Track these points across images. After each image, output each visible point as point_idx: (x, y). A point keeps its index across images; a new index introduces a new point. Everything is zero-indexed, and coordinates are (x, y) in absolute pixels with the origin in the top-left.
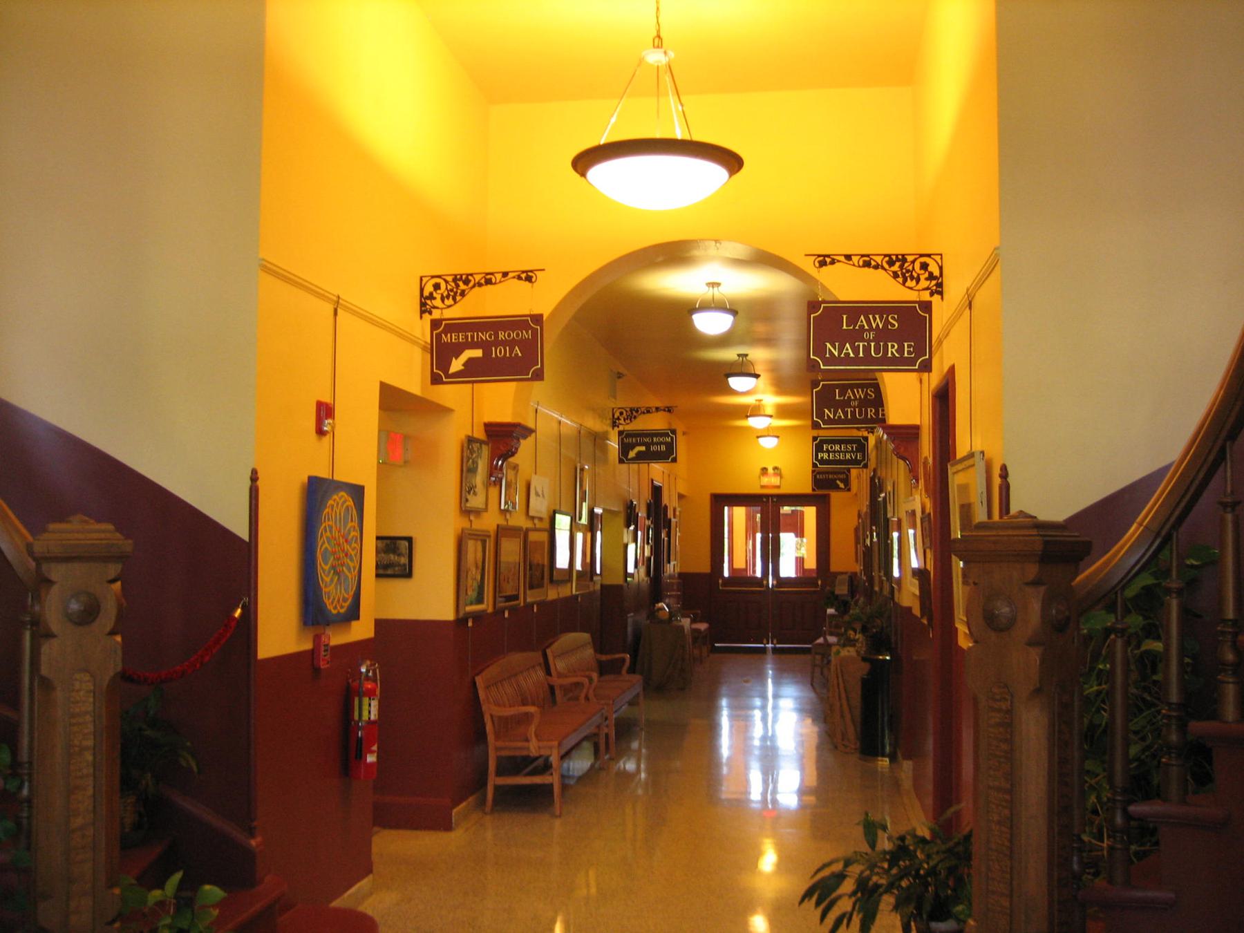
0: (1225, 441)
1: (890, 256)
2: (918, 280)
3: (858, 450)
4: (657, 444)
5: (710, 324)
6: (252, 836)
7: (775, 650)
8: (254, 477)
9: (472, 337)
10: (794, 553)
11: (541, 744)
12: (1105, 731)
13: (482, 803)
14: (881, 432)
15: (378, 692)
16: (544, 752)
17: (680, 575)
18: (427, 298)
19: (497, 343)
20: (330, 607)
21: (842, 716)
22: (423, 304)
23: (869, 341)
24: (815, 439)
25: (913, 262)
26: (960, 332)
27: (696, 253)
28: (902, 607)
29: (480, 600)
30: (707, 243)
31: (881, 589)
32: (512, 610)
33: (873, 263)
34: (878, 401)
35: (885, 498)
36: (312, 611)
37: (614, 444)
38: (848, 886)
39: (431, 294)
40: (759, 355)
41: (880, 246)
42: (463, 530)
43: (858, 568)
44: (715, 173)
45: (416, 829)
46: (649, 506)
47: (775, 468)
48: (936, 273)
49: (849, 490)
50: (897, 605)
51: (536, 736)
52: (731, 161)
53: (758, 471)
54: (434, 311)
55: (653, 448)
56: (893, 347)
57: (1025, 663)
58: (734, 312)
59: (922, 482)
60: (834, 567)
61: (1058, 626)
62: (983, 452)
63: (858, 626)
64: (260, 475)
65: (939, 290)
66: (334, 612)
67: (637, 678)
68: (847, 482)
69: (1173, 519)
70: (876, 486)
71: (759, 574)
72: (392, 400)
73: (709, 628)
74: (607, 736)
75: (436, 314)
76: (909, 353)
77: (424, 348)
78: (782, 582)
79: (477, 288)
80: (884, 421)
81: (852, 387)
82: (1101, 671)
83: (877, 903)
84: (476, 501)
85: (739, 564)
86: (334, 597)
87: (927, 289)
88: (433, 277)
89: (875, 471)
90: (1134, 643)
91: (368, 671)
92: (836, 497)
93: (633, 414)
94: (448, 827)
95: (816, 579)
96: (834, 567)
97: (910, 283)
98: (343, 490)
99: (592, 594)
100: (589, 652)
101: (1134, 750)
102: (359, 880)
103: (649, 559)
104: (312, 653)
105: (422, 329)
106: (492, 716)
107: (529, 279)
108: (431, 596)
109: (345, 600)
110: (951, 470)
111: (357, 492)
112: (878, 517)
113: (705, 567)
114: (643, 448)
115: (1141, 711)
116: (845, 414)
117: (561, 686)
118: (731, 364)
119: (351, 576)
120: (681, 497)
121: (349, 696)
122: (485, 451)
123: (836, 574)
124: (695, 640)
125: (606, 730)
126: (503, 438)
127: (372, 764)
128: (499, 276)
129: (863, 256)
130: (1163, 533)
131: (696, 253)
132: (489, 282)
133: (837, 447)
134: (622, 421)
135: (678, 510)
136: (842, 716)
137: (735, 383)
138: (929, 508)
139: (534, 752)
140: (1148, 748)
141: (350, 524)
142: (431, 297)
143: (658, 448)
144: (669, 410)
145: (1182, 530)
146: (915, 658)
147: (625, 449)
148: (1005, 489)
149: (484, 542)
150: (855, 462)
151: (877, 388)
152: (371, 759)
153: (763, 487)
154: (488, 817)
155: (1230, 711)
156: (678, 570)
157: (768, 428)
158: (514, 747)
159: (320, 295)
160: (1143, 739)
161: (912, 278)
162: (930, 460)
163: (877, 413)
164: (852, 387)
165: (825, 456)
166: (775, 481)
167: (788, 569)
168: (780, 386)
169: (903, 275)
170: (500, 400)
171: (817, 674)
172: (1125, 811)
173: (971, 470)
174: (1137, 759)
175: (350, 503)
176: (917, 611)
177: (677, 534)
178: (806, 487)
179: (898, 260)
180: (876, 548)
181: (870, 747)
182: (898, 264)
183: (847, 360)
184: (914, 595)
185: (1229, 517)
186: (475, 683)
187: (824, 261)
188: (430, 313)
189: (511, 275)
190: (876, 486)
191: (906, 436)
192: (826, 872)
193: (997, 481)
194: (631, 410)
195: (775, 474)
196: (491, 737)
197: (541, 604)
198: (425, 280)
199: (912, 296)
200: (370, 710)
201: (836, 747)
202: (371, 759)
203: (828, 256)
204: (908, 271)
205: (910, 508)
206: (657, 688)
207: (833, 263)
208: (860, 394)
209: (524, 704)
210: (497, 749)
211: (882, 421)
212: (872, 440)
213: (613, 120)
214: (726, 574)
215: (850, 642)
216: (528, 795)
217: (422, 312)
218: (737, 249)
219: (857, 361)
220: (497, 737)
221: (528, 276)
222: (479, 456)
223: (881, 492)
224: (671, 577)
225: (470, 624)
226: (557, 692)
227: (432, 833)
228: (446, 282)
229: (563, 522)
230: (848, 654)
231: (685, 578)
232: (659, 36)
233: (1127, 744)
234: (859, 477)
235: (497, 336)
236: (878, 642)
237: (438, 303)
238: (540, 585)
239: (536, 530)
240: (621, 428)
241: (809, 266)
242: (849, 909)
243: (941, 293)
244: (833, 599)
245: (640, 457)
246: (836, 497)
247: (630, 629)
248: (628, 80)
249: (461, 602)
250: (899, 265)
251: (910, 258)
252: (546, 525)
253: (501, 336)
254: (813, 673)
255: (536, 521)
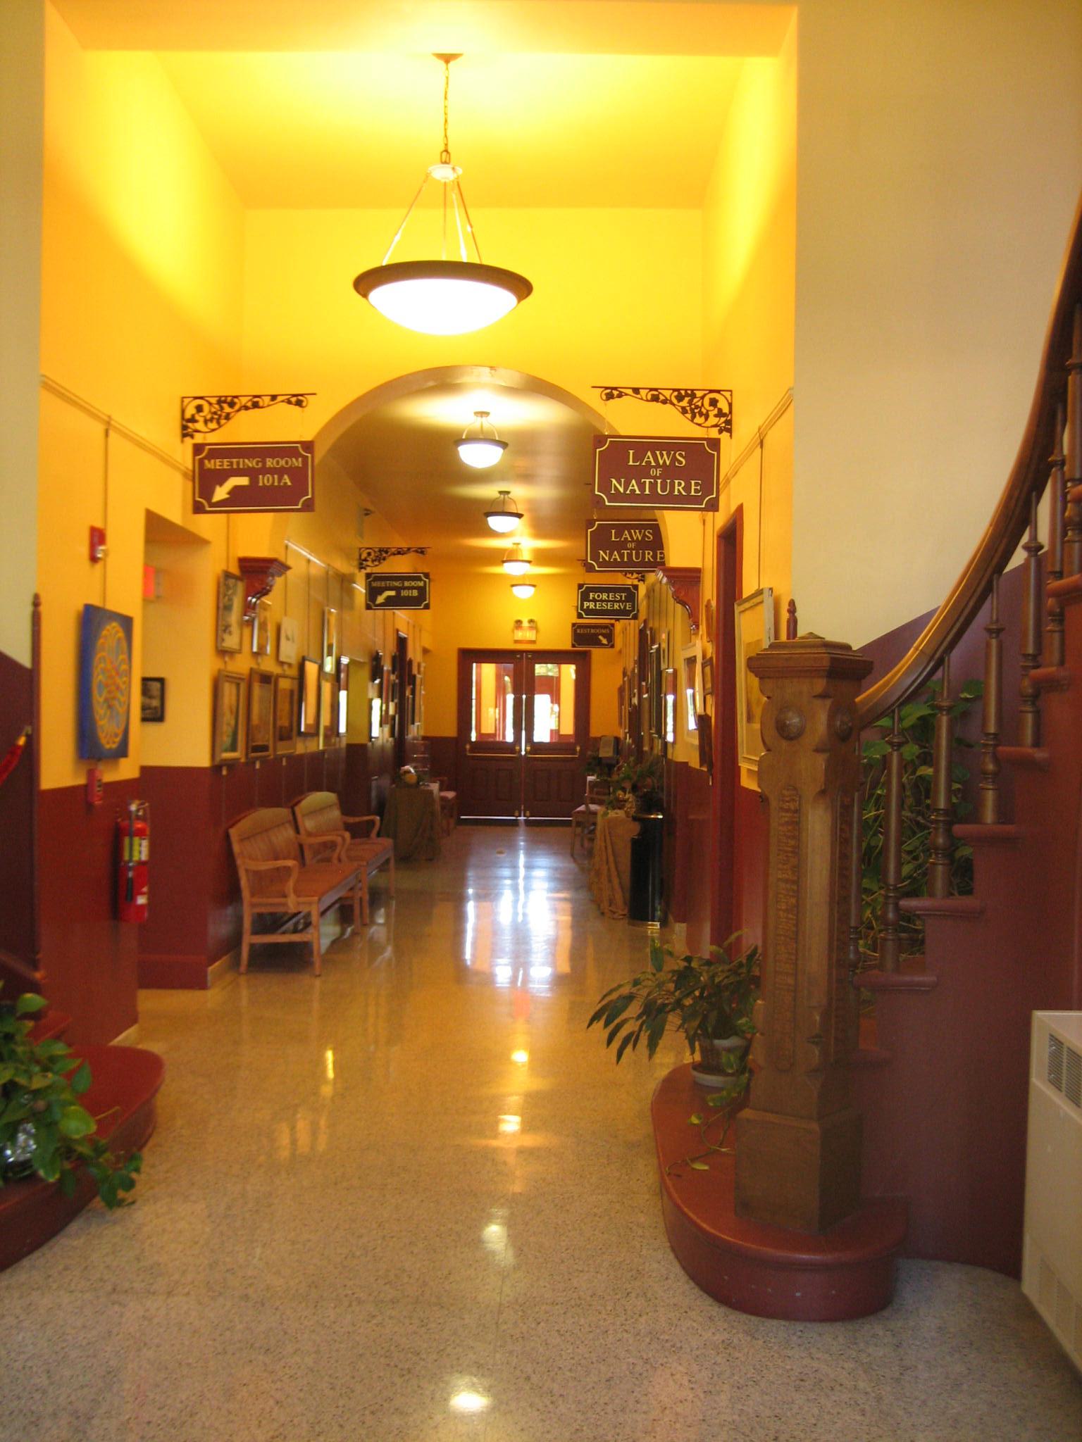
0: (993, 573)
1: (678, 390)
2: (707, 417)
3: (626, 601)
4: (408, 588)
5: (475, 456)
6: (36, 967)
7: (528, 823)
8: (36, 603)
9: (238, 463)
10: (550, 718)
11: (302, 900)
12: (880, 853)
13: (236, 963)
14: (661, 575)
15: (148, 832)
16: (305, 910)
17: (424, 738)
18: (189, 421)
19: (265, 471)
20: (103, 741)
21: (610, 881)
22: (184, 428)
23: (655, 478)
24: (580, 586)
25: (702, 398)
26: (750, 469)
27: (465, 379)
28: (677, 763)
29: (233, 748)
30: (477, 370)
31: (652, 749)
32: (264, 761)
33: (662, 398)
34: (656, 542)
35: (658, 650)
36: (88, 747)
37: (360, 588)
38: (634, 1009)
39: (193, 416)
40: (520, 493)
41: (668, 381)
42: (219, 671)
43: (621, 733)
44: (502, 297)
45: (173, 988)
46: (394, 659)
47: (531, 621)
48: (726, 410)
49: (612, 646)
50: (669, 762)
51: (295, 891)
52: (520, 286)
53: (512, 624)
54: (197, 435)
55: (404, 593)
56: (680, 484)
57: (811, 767)
58: (504, 445)
59: (703, 628)
60: (595, 732)
61: (843, 738)
62: (771, 589)
63: (628, 785)
64: (43, 600)
65: (727, 427)
66: (108, 747)
67: (388, 842)
68: (610, 637)
69: (945, 644)
70: (645, 638)
71: (510, 738)
72: (158, 531)
73: (457, 797)
74: (361, 899)
75: (199, 439)
76: (696, 491)
77: (185, 475)
78: (537, 748)
79: (243, 412)
80: (663, 564)
81: (629, 528)
82: (880, 796)
83: (664, 1021)
84: (231, 642)
85: (488, 728)
86: (107, 733)
87: (716, 426)
88: (196, 398)
89: (645, 622)
90: (910, 771)
91: (138, 810)
92: (597, 653)
93: (382, 554)
94: (203, 986)
95: (575, 744)
96: (595, 732)
97: (699, 420)
98: (115, 620)
99: (337, 751)
100: (336, 813)
101: (906, 870)
102: (126, 1029)
103: (393, 718)
104: (85, 788)
105: (183, 454)
106: (247, 871)
107: (299, 403)
108: (185, 741)
109: (116, 735)
110: (737, 609)
111: (126, 622)
112: (649, 674)
113: (449, 729)
114: (392, 593)
115: (914, 834)
116: (622, 556)
117: (310, 846)
118: (493, 502)
119: (122, 710)
120: (425, 651)
121: (118, 836)
122: (241, 587)
123: (598, 740)
124: (443, 808)
125: (360, 894)
126: (256, 574)
127: (142, 906)
128: (267, 399)
129: (651, 390)
130: (937, 656)
131: (465, 379)
132: (256, 405)
133: (604, 596)
134: (369, 563)
135: (423, 665)
136: (610, 881)
137: (495, 522)
138: (710, 650)
139: (292, 909)
140: (920, 866)
141: (121, 657)
142: (193, 420)
143: (410, 594)
144: (421, 551)
145: (954, 652)
146: (691, 817)
147: (373, 593)
148: (793, 622)
149: (238, 685)
150: (624, 613)
151: (656, 530)
152: (141, 900)
153: (516, 642)
154: (243, 980)
155: (989, 815)
156: (422, 733)
157: (524, 576)
158: (268, 904)
159: (94, 415)
160: (916, 858)
161: (701, 414)
162: (714, 603)
163: (654, 556)
164: (629, 528)
165: (592, 605)
166: (530, 635)
167: (542, 734)
168: (540, 529)
169: (692, 410)
170: (257, 533)
171: (578, 846)
172: (896, 906)
173: (759, 608)
174: (910, 877)
175: (121, 634)
176: (695, 762)
177: (421, 691)
178: (564, 642)
179: (687, 395)
180: (646, 705)
181: (639, 911)
182: (687, 399)
183: (632, 497)
184: (692, 745)
185: (994, 642)
186: (228, 836)
187: (612, 393)
188: (192, 437)
189: (280, 398)
190: (645, 638)
191: (686, 580)
192: (614, 996)
193: (785, 616)
194: (381, 550)
195: (531, 628)
196: (246, 893)
197: (290, 758)
198: (186, 401)
199: (698, 432)
200: (140, 850)
201: (603, 914)
202: (141, 900)
203: (615, 389)
204: (697, 407)
205: (689, 654)
206: (406, 858)
207: (620, 396)
208: (637, 535)
209: (276, 859)
210: (253, 905)
211: (659, 564)
212: (642, 590)
213: (397, 239)
214: (474, 737)
215: (619, 804)
216: (284, 959)
217: (184, 435)
218: (508, 377)
219: (643, 498)
220: (253, 895)
221: (298, 401)
222: (234, 593)
223: (653, 643)
224: (414, 738)
225: (224, 772)
226: (308, 854)
227: (186, 992)
228: (210, 404)
229: (311, 669)
230: (616, 820)
231: (433, 744)
232: (446, 151)
233: (899, 865)
234: (624, 630)
235: (264, 463)
236: (649, 802)
237: (369, 563)
238: (290, 738)
239: (285, 677)
240: (369, 570)
241: (594, 400)
242: (636, 1029)
243: (729, 431)
244: (600, 765)
245: (390, 602)
246: (597, 653)
247: (374, 794)
248: (413, 193)
249: (217, 745)
250: (688, 400)
251: (699, 394)
252: (294, 672)
253: (270, 463)
254: (572, 849)
255: (286, 667)
